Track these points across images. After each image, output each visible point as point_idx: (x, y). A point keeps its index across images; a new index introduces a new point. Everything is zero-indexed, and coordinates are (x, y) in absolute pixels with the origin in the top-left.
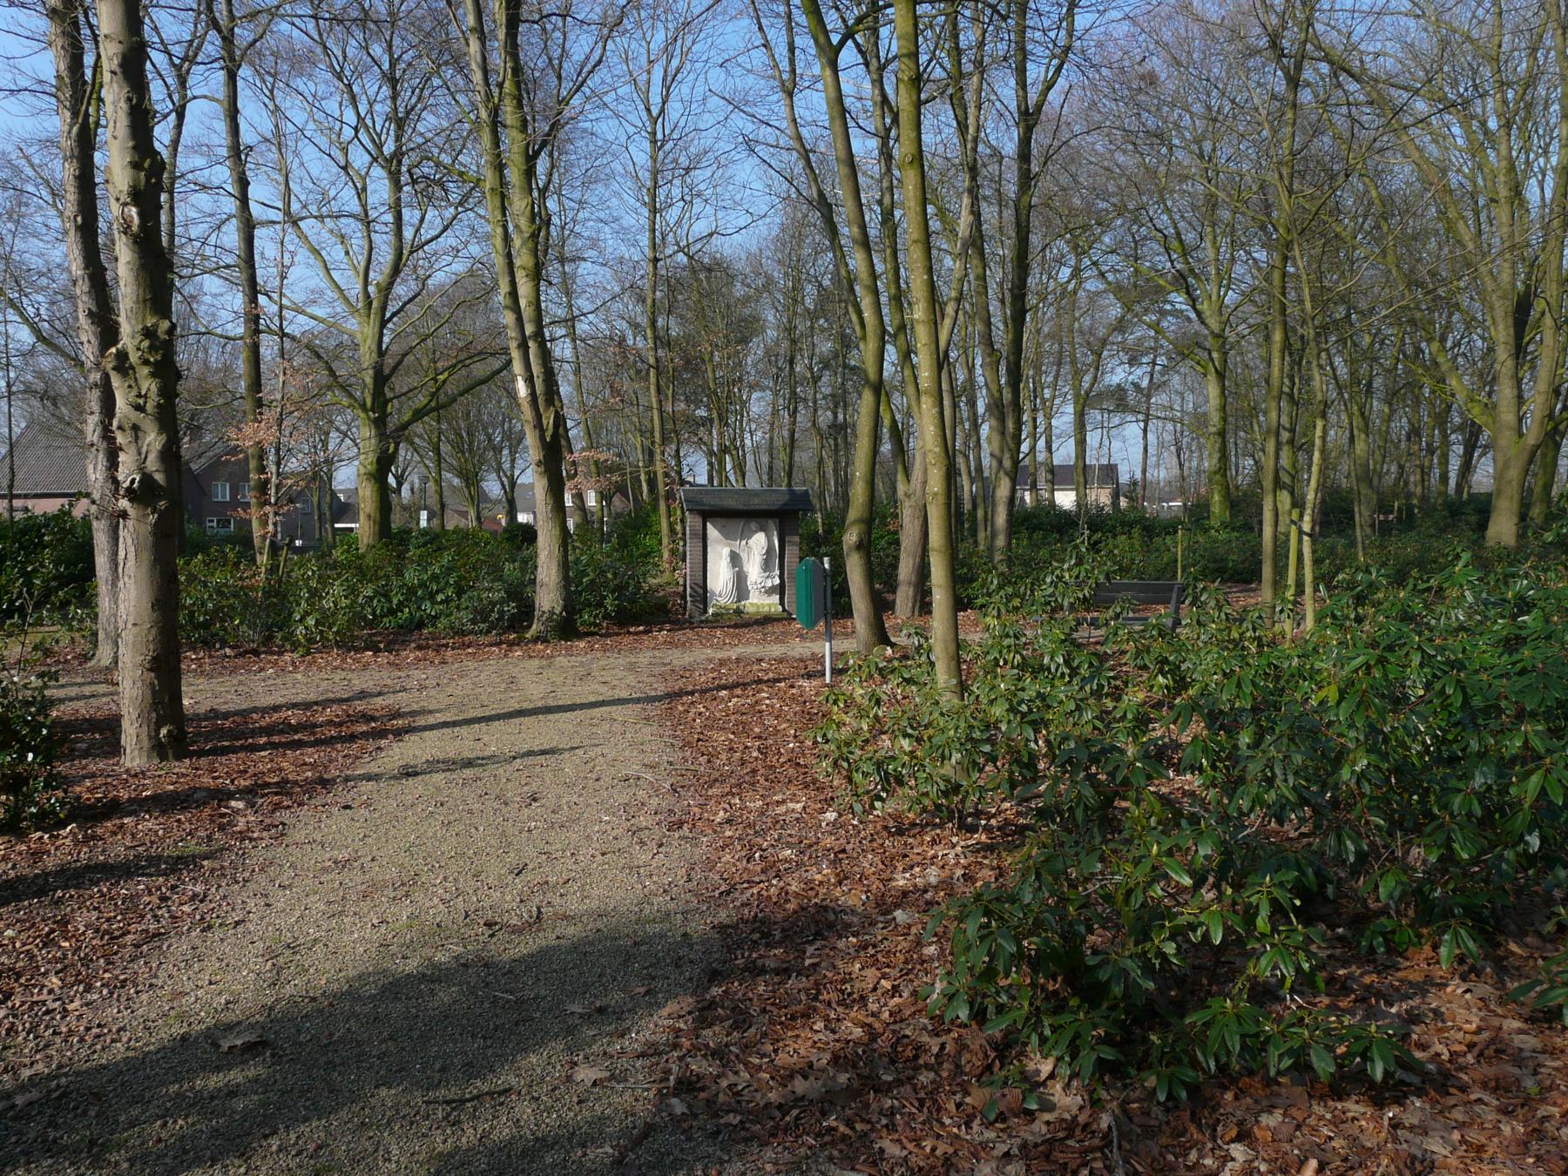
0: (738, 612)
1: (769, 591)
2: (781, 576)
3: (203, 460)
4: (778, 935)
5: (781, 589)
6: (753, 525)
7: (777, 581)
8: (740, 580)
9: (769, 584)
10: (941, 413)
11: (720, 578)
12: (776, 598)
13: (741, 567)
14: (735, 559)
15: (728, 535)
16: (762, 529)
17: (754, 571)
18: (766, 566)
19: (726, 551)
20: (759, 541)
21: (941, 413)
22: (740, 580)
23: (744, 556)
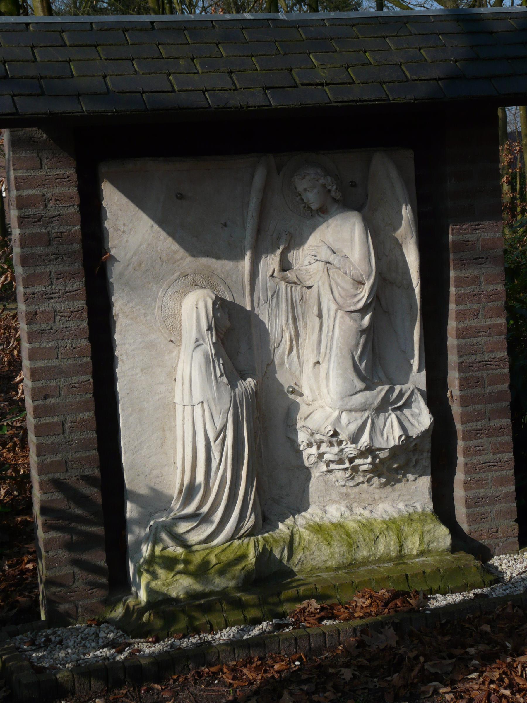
0: (268, 580)
1: (390, 467)
2: (436, 397)
3: (461, 237)
4: (42, 645)
5: (435, 453)
6: (309, 186)
7: (421, 419)
8: (265, 427)
9: (391, 435)
10: (40, 114)
11: (174, 422)
12: (417, 490)
13: (266, 371)
14: (237, 341)
15: (199, 233)
16: (351, 198)
17: (323, 390)
18: (374, 361)
19: (194, 309)
20: (336, 255)
21: (40, 114)
22: (265, 427)
23: (276, 323)
